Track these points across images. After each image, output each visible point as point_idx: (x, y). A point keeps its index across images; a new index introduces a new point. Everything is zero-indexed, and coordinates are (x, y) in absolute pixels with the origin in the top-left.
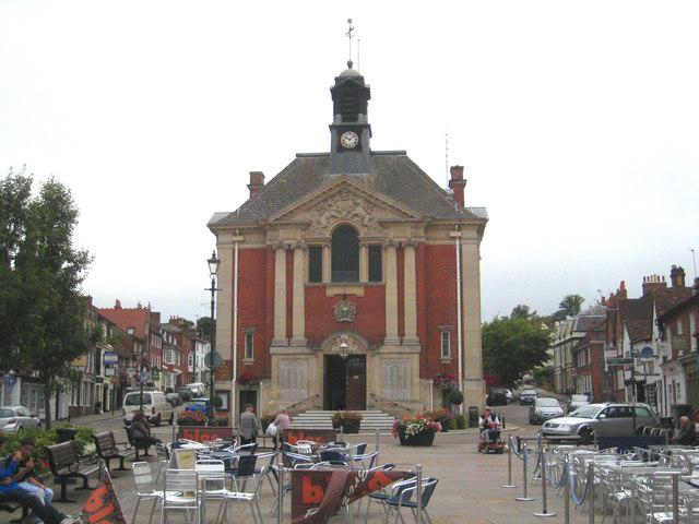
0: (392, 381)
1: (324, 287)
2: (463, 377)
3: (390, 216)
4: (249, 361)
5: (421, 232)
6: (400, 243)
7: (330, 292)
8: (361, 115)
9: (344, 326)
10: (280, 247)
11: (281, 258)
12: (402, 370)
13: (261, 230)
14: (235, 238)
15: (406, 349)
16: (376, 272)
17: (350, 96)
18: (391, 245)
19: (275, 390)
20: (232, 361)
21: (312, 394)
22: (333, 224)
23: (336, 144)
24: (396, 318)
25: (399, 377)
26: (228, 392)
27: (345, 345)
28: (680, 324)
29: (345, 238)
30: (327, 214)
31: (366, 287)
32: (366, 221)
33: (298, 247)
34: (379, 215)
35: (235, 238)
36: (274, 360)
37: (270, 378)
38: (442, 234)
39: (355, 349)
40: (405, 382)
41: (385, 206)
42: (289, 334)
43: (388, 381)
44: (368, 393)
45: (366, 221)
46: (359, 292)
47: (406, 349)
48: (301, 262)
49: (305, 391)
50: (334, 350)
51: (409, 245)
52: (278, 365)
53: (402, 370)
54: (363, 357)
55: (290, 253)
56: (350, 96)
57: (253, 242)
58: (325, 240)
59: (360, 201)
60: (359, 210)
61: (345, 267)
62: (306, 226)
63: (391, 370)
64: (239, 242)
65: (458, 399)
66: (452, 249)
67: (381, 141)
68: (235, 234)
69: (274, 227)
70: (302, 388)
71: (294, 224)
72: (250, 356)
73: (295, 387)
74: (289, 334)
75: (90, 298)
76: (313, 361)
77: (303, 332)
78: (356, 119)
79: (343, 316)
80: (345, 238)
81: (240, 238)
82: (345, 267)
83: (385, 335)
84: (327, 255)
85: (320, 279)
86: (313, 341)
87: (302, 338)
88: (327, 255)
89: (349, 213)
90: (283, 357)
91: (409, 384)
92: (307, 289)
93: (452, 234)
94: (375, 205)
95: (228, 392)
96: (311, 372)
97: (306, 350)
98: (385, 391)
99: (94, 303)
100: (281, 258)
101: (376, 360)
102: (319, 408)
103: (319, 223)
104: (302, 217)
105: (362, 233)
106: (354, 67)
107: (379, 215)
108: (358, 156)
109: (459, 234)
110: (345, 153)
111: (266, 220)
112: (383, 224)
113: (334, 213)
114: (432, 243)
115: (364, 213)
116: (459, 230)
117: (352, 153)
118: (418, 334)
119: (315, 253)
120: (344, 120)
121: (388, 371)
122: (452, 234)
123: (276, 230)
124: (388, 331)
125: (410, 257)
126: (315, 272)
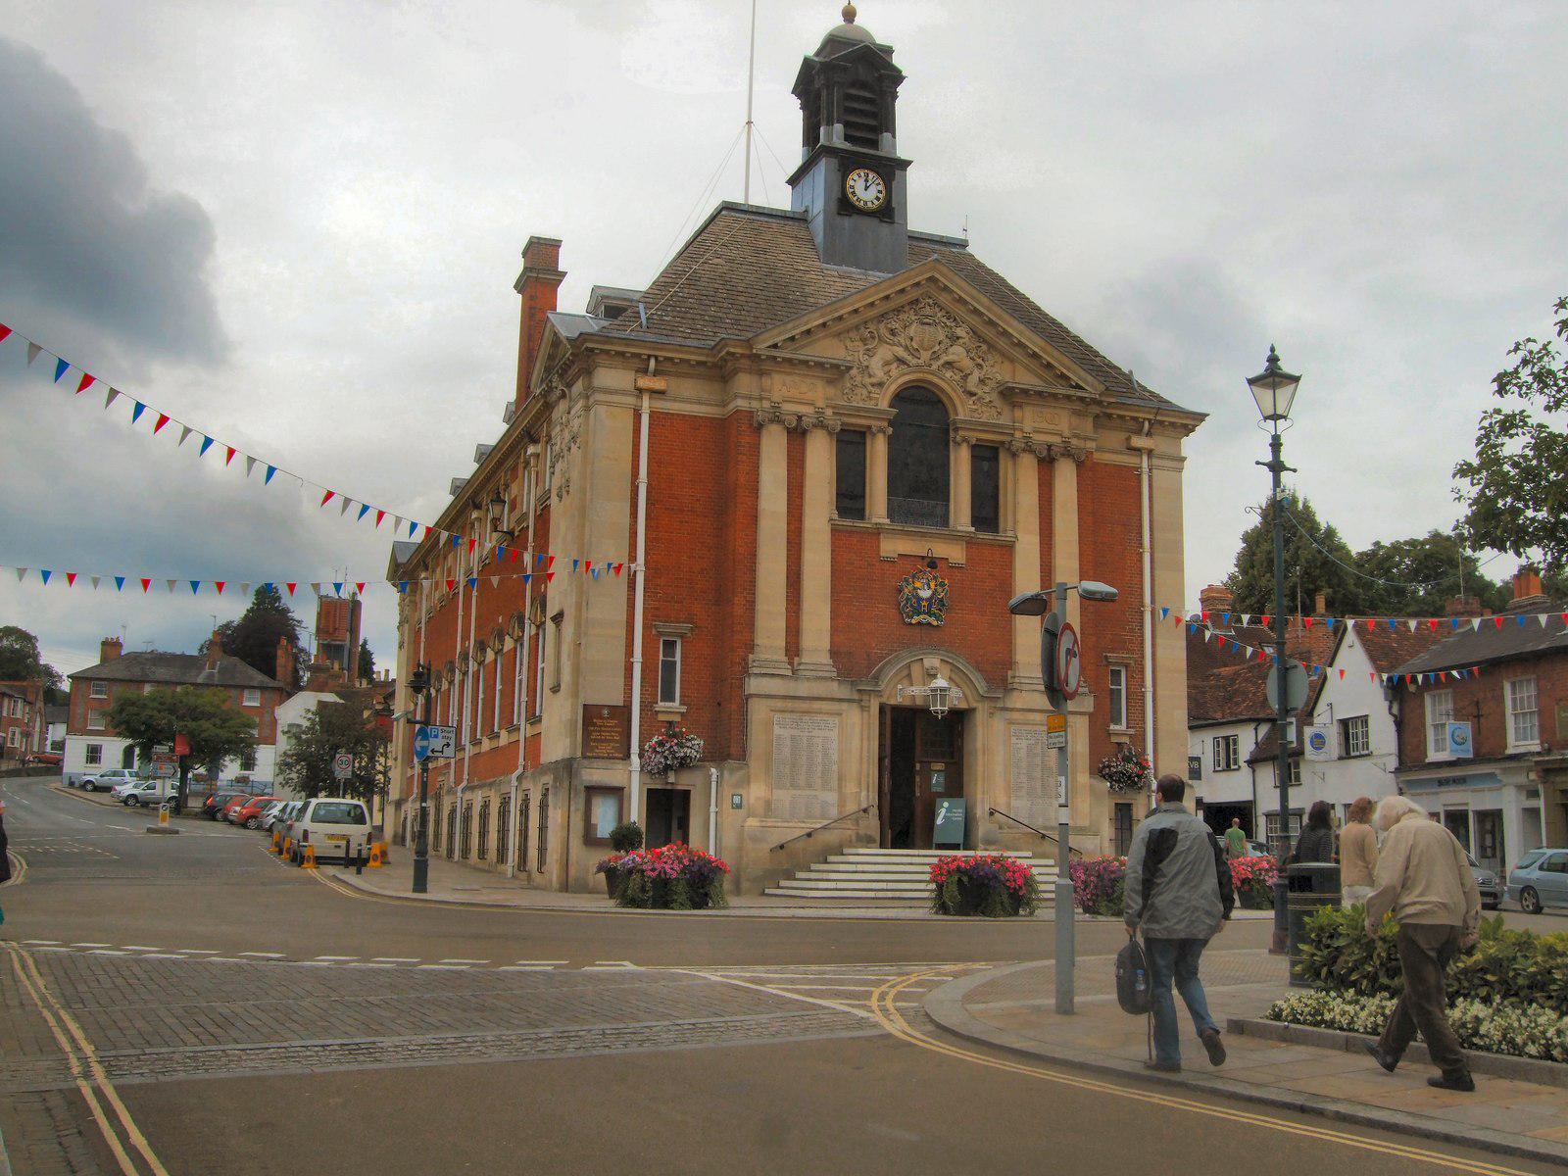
0: (1030, 778)
1: (877, 532)
3: (1026, 379)
6: (1050, 447)
7: (892, 547)
8: (887, 135)
13: (719, 370)
14: (644, 382)
15: (803, 688)
16: (987, 511)
18: (1029, 449)
19: (756, 792)
20: (627, 708)
21: (851, 807)
22: (899, 379)
23: (836, 194)
27: (933, 682)
29: (921, 412)
30: (884, 352)
31: (970, 542)
32: (972, 383)
34: (1002, 372)
35: (644, 382)
36: (758, 711)
37: (743, 756)
39: (956, 699)
41: (1017, 353)
42: (793, 648)
43: (1023, 779)
45: (972, 383)
48: (821, 458)
49: (831, 797)
50: (911, 693)
52: (767, 725)
55: (797, 435)
56: (850, 93)
57: (690, 399)
58: (876, 413)
60: (957, 353)
61: (920, 492)
62: (835, 372)
63: (1029, 749)
67: (927, 209)
69: (759, 365)
70: (825, 786)
71: (820, 365)
73: (809, 786)
74: (793, 648)
75: (1270, 445)
76: (853, 717)
80: (921, 412)
81: (658, 384)
82: (920, 492)
84: (878, 453)
85: (860, 514)
86: (854, 665)
87: (825, 659)
88: (878, 453)
89: (935, 356)
90: (780, 704)
93: (1138, 442)
94: (991, 347)
95: (617, 792)
96: (844, 749)
97: (835, 689)
98: (1014, 803)
100: (773, 449)
101: (998, 724)
102: (868, 841)
103: (865, 370)
104: (829, 350)
105: (962, 411)
106: (858, 21)
107: (1002, 372)
108: (884, 230)
110: (855, 218)
111: (749, 343)
112: (1011, 396)
113: (901, 352)
115: (967, 363)
119: (851, 444)
121: (1023, 753)
123: (761, 373)
126: (850, 497)
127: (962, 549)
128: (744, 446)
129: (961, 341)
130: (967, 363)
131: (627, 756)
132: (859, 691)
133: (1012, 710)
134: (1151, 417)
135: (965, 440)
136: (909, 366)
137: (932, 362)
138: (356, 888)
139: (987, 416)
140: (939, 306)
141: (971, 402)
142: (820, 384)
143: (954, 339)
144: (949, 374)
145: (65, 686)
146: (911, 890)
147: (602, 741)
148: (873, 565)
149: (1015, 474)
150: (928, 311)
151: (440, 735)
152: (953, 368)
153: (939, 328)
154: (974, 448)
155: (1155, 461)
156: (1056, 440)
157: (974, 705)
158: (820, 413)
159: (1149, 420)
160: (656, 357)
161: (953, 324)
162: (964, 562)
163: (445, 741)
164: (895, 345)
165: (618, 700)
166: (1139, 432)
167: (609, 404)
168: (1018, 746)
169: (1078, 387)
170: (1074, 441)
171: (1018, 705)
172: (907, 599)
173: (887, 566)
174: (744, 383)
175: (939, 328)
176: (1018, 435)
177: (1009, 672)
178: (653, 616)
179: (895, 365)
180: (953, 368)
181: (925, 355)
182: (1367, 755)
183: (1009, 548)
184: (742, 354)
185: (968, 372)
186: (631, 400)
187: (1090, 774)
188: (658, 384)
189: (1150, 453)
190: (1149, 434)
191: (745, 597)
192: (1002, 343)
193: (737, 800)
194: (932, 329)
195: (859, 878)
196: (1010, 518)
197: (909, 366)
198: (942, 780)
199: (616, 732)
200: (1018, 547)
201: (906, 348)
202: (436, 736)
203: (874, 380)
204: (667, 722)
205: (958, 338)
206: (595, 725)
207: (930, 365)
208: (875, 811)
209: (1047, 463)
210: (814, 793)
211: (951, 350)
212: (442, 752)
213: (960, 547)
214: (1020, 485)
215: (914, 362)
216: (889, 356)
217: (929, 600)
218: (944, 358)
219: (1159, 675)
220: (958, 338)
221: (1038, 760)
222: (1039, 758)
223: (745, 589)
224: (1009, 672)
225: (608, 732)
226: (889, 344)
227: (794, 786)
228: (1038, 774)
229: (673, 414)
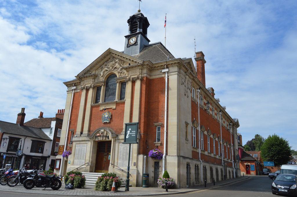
17: (138, 24)
20: (64, 146)
26: (60, 160)
28: (104, 139)
38: (157, 72)
56: (138, 24)
58: (101, 82)
59: (117, 61)
66: (163, 79)
81: (75, 88)
93: (163, 71)
99: (238, 129)
109: (167, 70)
114: (154, 77)
116: (167, 68)
117: (133, 46)
119: (98, 89)
124: (77, 130)
125: (138, 84)
126: (96, 99)
159: (166, 65)
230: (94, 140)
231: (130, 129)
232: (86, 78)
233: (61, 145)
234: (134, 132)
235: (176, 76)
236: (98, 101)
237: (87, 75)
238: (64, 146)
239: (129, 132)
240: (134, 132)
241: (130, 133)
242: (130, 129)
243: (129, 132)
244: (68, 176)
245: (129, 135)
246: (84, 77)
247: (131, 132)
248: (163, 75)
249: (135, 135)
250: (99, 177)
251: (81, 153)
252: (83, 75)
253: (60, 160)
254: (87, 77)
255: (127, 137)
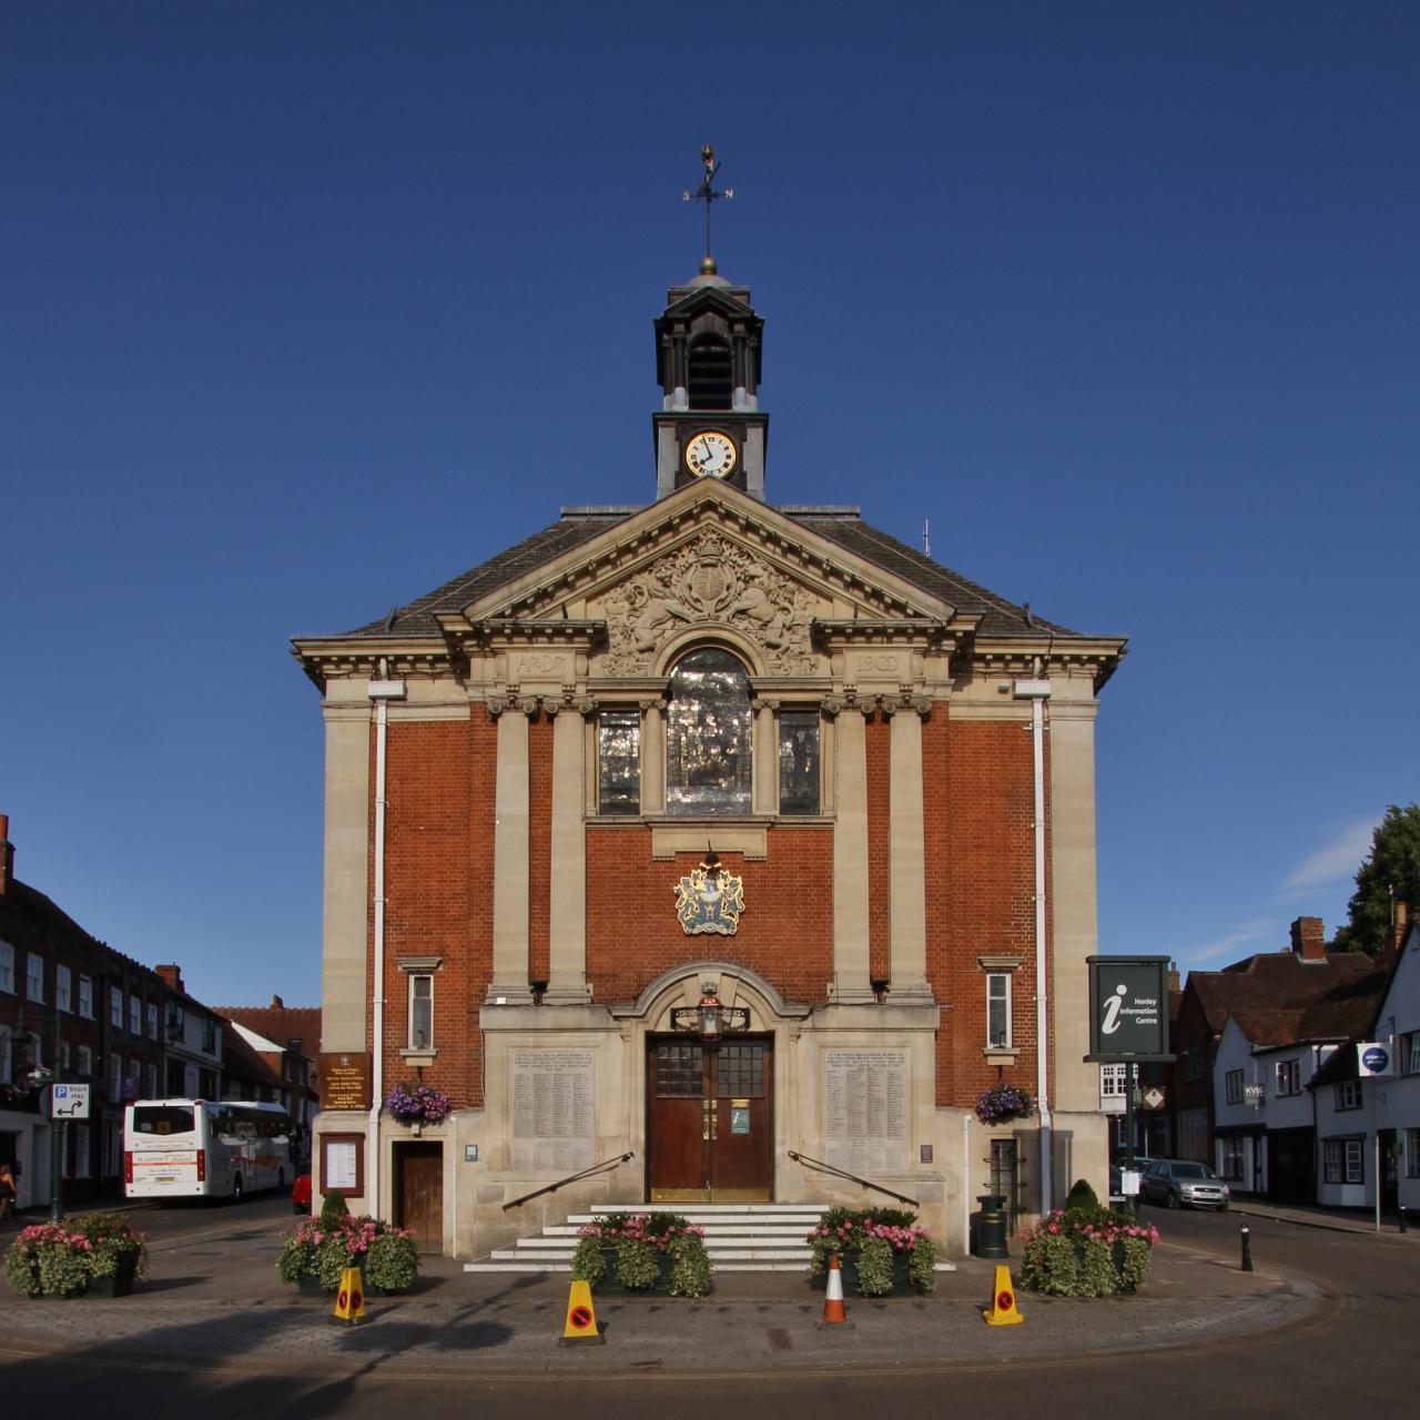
0: (852, 1113)
2: (1051, 1107)
3: (838, 611)
4: (418, 1057)
5: (940, 667)
9: (710, 947)
10: (513, 705)
11: (513, 733)
12: (883, 1079)
18: (851, 704)
24: (863, 922)
25: (873, 1102)
26: (358, 1139)
33: (569, 705)
36: (494, 1045)
40: (892, 1117)
43: (842, 1114)
44: (780, 1151)
46: (754, 843)
47: (895, 1019)
51: (906, 704)
53: (883, 1079)
54: (768, 1038)
60: (754, 598)
62: (598, 639)
64: (391, 700)
65: (748, 1165)
68: (376, 676)
71: (559, 631)
72: (423, 1041)
73: (558, 1132)
77: (582, 967)
78: (728, 405)
79: (702, 919)
81: (395, 688)
83: (830, 975)
86: (613, 991)
89: (723, 605)
91: (903, 1121)
92: (591, 830)
93: (1024, 687)
94: (801, 583)
96: (610, 1079)
100: (513, 733)
103: (628, 633)
104: (580, 612)
112: (823, 638)
113: (674, 605)
118: (930, 976)
120: (693, 404)
121: (842, 1083)
122: (1024, 687)
124: (839, 966)
125: (906, 735)
127: (763, 839)
128: (477, 744)
129: (757, 580)
130: (764, 608)
131: (369, 1106)
132: (616, 1018)
133: (825, 1030)
134: (1043, 651)
135: (766, 705)
136: (688, 622)
137: (719, 614)
138: (1076, 1113)
139: (796, 669)
140: (728, 542)
141: (774, 657)
142: (569, 657)
143: (749, 579)
144: (743, 625)
145: (1172, 1058)
146: (756, 1236)
147: (342, 1092)
148: (645, 868)
149: (835, 738)
150: (710, 548)
151: (69, 1094)
152: (749, 616)
153: (726, 568)
154: (776, 713)
155: (1052, 710)
156: (893, 690)
157: (772, 1027)
158: (569, 692)
159: (1041, 656)
160: (386, 657)
161: (747, 562)
162: (765, 854)
163: (75, 1101)
164: (666, 597)
165: (361, 1048)
166: (1028, 675)
167: (339, 719)
168: (836, 1074)
169: (917, 615)
170: (917, 689)
171: (833, 1024)
172: (688, 905)
173: (662, 867)
174: (480, 667)
175: (726, 568)
176: (838, 689)
177: (829, 986)
178: (397, 951)
179: (669, 624)
180: (749, 616)
181: (709, 607)
182: (435, 1255)
183: (826, 832)
184: (463, 632)
185: (768, 619)
186: (367, 712)
187: (937, 1105)
188: (395, 688)
189: (1045, 698)
190: (1043, 676)
191: (482, 919)
192: (813, 574)
193: (471, 1151)
194: (715, 571)
195: (557, 1253)
196: (829, 796)
197: (688, 622)
198: (746, 1119)
199: (356, 1081)
200: (838, 828)
201: (684, 601)
202: (64, 1096)
203: (642, 645)
204: (996, 1066)
205: (753, 577)
206: (333, 1075)
207: (717, 619)
208: (639, 1159)
209: (878, 717)
210: (562, 1140)
211: (744, 594)
212: (72, 1112)
213: (760, 836)
214: (843, 746)
215: (692, 616)
216: (661, 613)
217: (717, 904)
218: (737, 605)
219: (1058, 980)
220: (753, 577)
221: (863, 1091)
222: (865, 1089)
223: (482, 909)
224: (829, 986)
225: (348, 1081)
226: (658, 597)
227: (539, 1133)
228: (864, 1107)
229: (416, 723)
230: (650, 1027)
231: (1122, 989)
232: (520, 641)
233: (342, 1054)
234: (1151, 1007)
235: (1089, 727)
236: (1371, 860)
237: (527, 618)
238: (363, 1061)
239: (1115, 1002)
240: (1151, 1007)
241: (1123, 1006)
242: (1122, 989)
243: (1115, 1002)
244: (1236, 1154)
245: (1119, 1017)
246: (518, 631)
247: (1127, 1001)
248: (1019, 713)
249: (1155, 1021)
250: (823, 1214)
251: (559, 1105)
252: (502, 615)
253: (358, 1139)
254: (538, 632)
255: (1108, 1028)
